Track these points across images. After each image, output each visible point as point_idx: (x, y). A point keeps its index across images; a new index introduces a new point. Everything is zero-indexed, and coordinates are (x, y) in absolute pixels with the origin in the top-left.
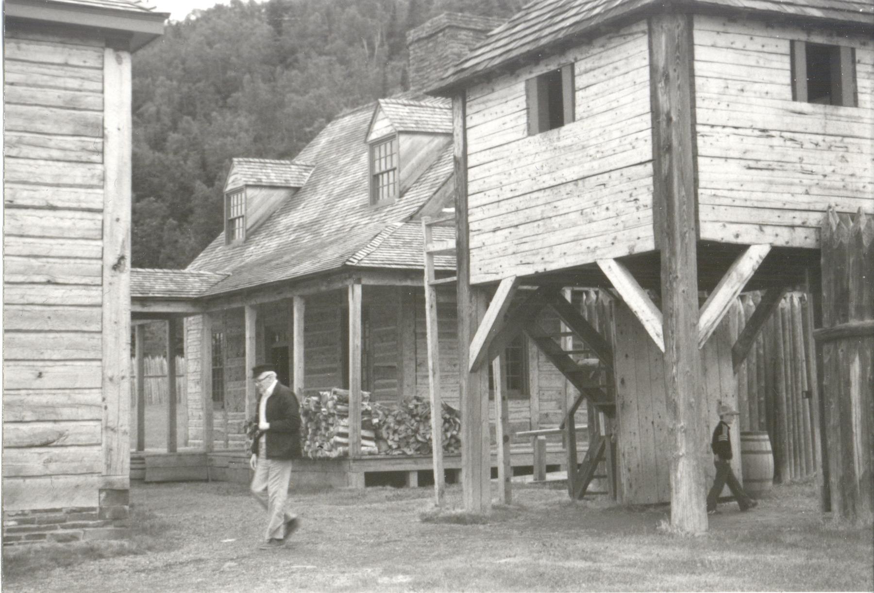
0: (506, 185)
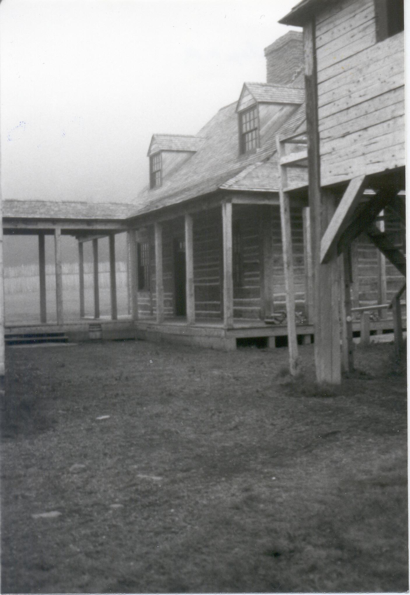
0: (355, 92)
